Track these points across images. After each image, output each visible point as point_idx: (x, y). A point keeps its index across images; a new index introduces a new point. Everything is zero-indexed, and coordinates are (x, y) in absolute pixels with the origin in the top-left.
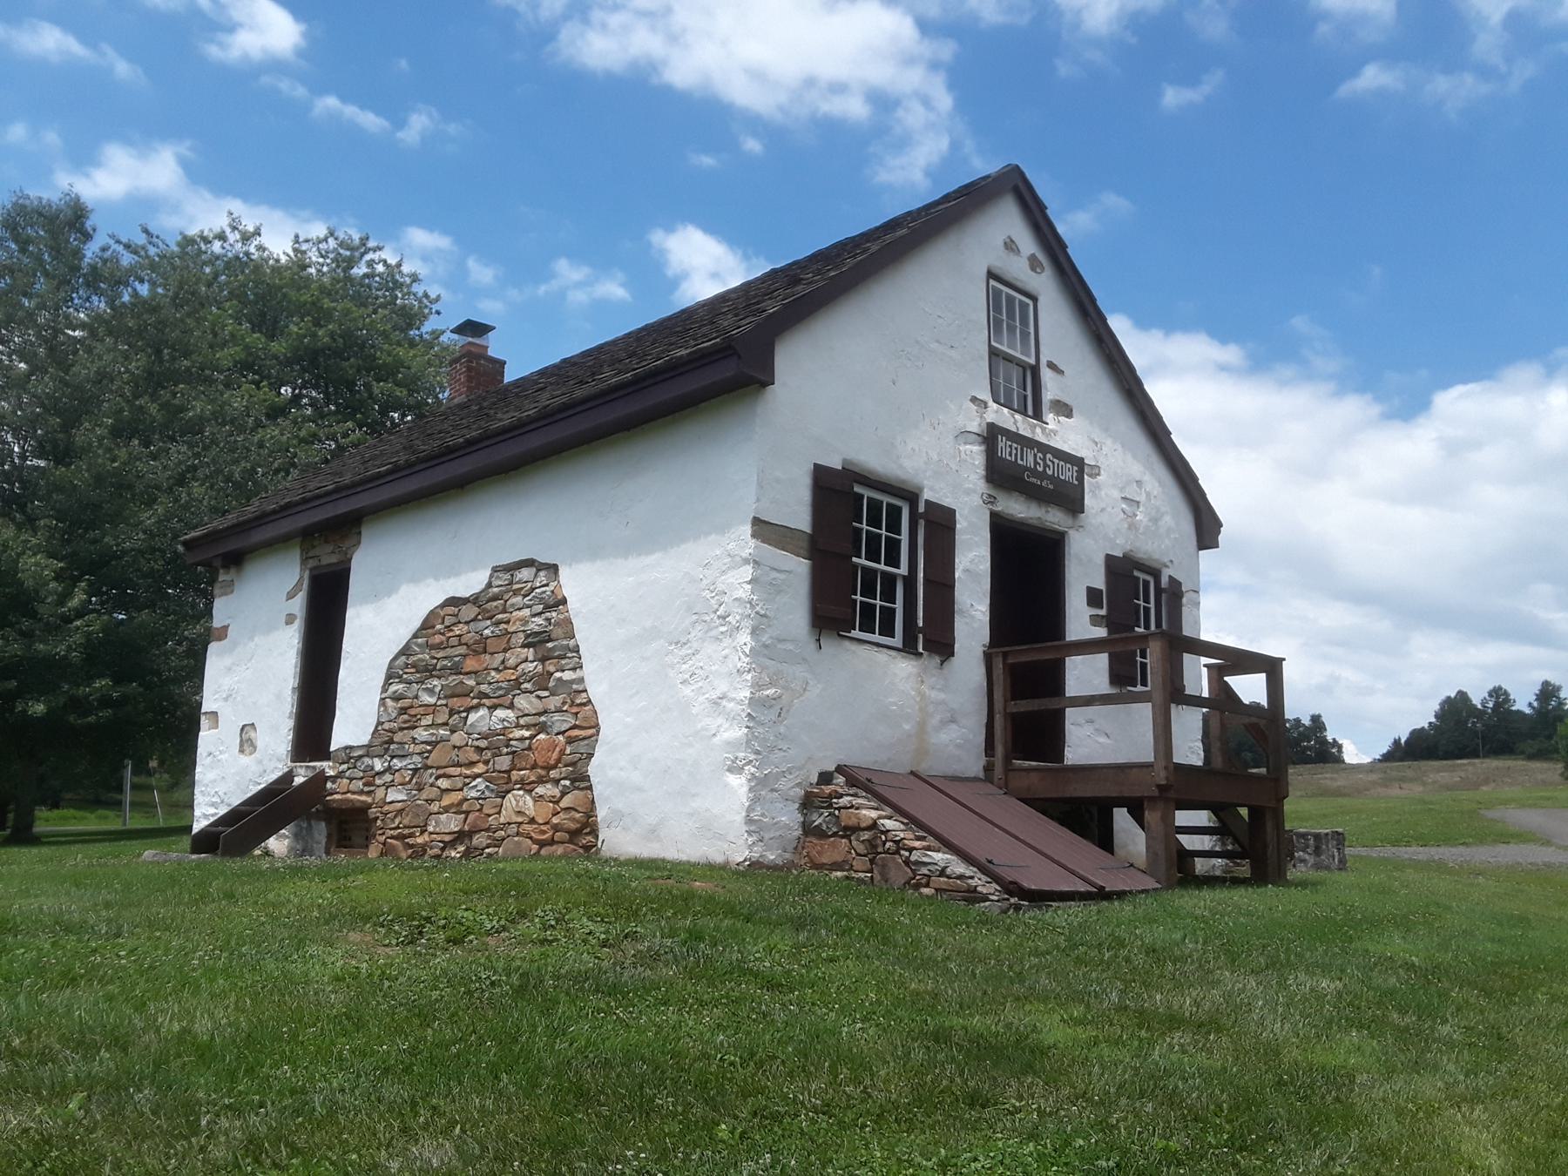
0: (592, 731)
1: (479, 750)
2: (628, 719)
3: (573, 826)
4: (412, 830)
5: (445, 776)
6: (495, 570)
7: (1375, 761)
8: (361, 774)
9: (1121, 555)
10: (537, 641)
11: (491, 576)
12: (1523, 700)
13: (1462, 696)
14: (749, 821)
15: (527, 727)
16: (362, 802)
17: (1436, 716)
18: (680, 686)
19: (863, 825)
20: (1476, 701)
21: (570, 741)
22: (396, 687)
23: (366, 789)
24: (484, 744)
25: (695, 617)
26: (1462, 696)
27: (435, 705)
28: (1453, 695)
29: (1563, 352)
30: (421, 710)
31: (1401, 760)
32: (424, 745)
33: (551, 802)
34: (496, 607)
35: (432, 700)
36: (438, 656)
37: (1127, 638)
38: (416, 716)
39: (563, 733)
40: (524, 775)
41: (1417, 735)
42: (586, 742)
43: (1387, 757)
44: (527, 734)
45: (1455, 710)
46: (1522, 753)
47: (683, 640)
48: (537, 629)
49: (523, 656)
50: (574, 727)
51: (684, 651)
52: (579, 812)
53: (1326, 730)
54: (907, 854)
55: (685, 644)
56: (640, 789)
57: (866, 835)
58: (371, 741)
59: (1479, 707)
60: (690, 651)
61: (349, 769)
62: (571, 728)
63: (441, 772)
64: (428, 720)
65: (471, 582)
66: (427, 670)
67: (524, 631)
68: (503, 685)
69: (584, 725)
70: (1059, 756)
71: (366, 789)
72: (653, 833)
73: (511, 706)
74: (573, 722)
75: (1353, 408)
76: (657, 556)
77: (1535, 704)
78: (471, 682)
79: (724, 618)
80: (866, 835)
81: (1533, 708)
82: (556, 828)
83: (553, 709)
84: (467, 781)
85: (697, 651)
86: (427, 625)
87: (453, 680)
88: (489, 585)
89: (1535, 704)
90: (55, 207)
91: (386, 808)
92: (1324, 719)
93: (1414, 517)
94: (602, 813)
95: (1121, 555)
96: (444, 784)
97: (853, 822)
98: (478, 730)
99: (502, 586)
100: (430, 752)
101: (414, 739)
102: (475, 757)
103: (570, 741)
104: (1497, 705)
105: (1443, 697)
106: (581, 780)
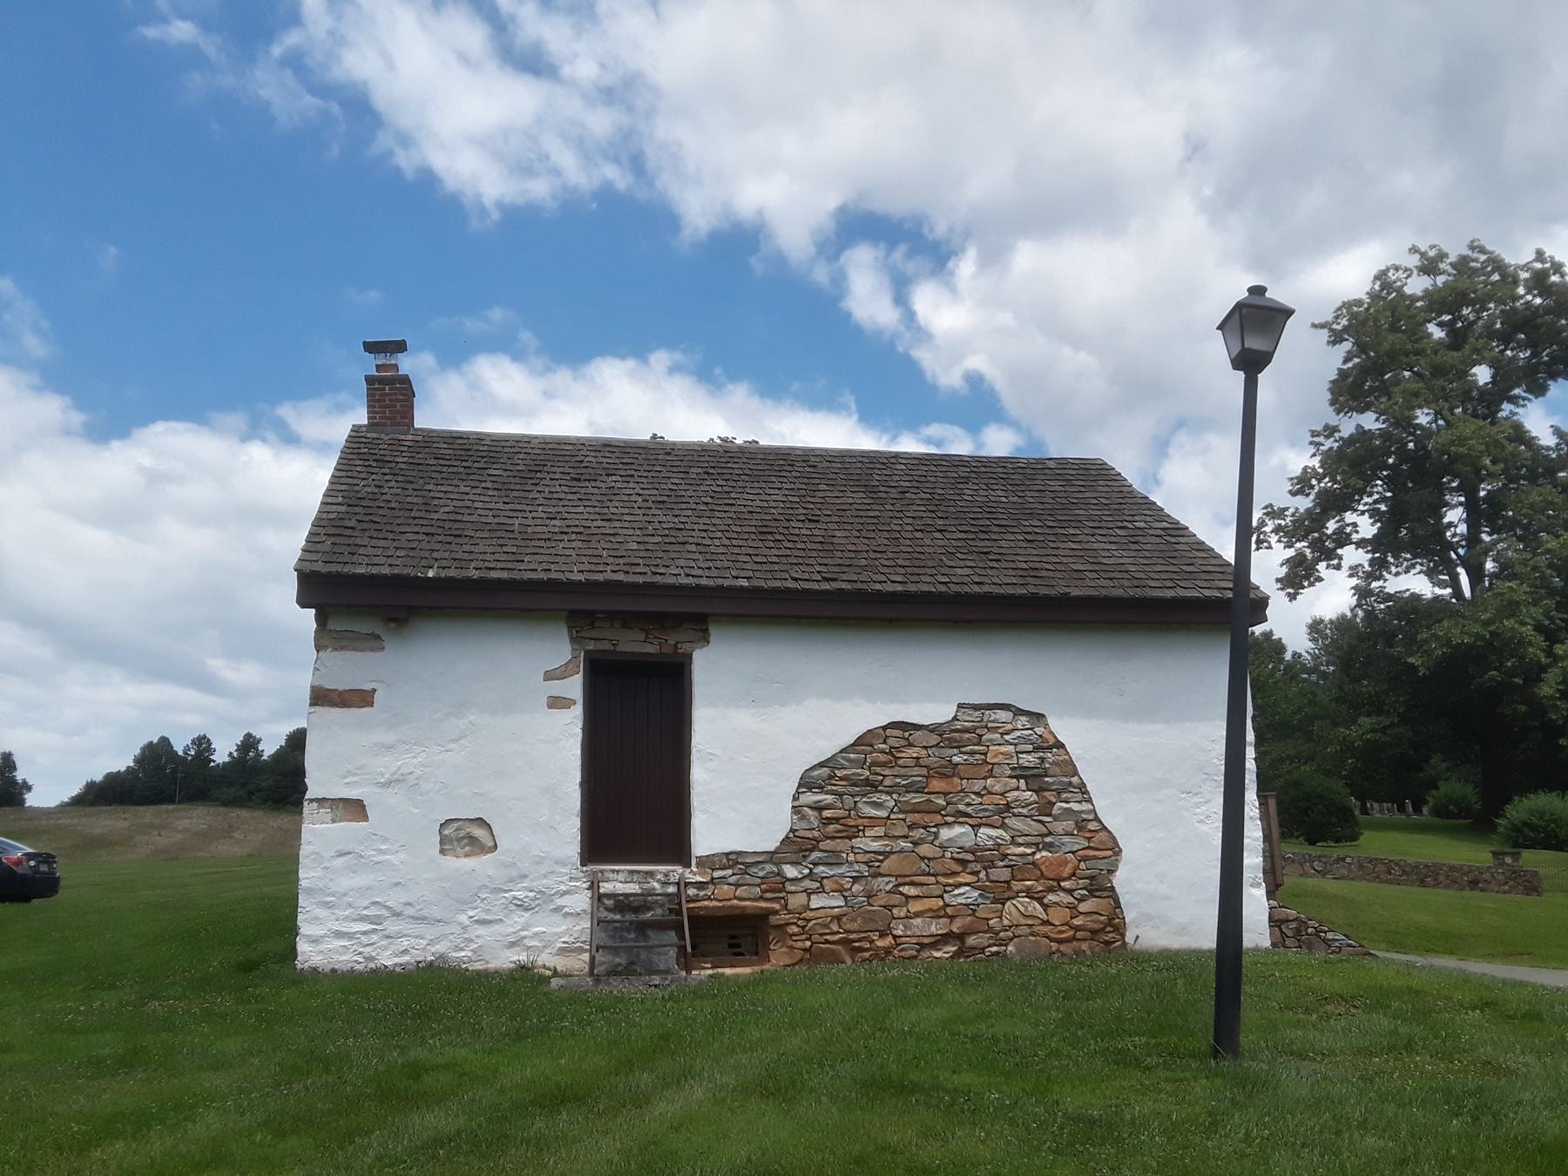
2: (1148, 845)
3: (1096, 926)
6: (960, 706)
7: (63, 806)
8: (759, 881)
11: (957, 711)
12: (223, 751)
13: (165, 741)
14: (1271, 919)
15: (1027, 845)
16: (761, 908)
17: (135, 761)
18: (1197, 824)
19: (1291, 918)
21: (1085, 859)
22: (809, 798)
25: (1205, 776)
26: (165, 741)
28: (155, 741)
31: (92, 804)
32: (872, 855)
33: (1067, 907)
34: (968, 739)
36: (885, 773)
39: (1073, 853)
40: (1033, 885)
41: (112, 778)
42: (1106, 861)
43: (78, 801)
44: (1029, 851)
45: (156, 755)
46: (217, 799)
47: (1196, 791)
48: (1027, 764)
51: (1196, 799)
52: (1102, 915)
53: (15, 769)
54: (1324, 935)
55: (1197, 794)
56: (1169, 898)
57: (1293, 925)
58: (778, 848)
59: (181, 753)
60: (1201, 800)
61: (734, 874)
62: (1083, 849)
65: (936, 711)
66: (873, 786)
67: (1008, 764)
68: (990, 807)
69: (1101, 847)
70: (675, 845)
72: (1183, 930)
73: (1003, 826)
74: (1087, 845)
75: (51, 408)
76: (1160, 726)
77: (235, 754)
78: (941, 802)
80: (1293, 925)
81: (233, 757)
82: (1077, 929)
83: (1062, 832)
85: (1210, 801)
88: (955, 718)
89: (235, 754)
90: (496, 216)
91: (809, 914)
92: (15, 758)
93: (97, 538)
94: (1129, 915)
96: (912, 891)
97: (1283, 917)
99: (973, 721)
100: (881, 861)
101: (852, 847)
102: (959, 869)
103: (1085, 859)
104: (199, 753)
105: (145, 742)
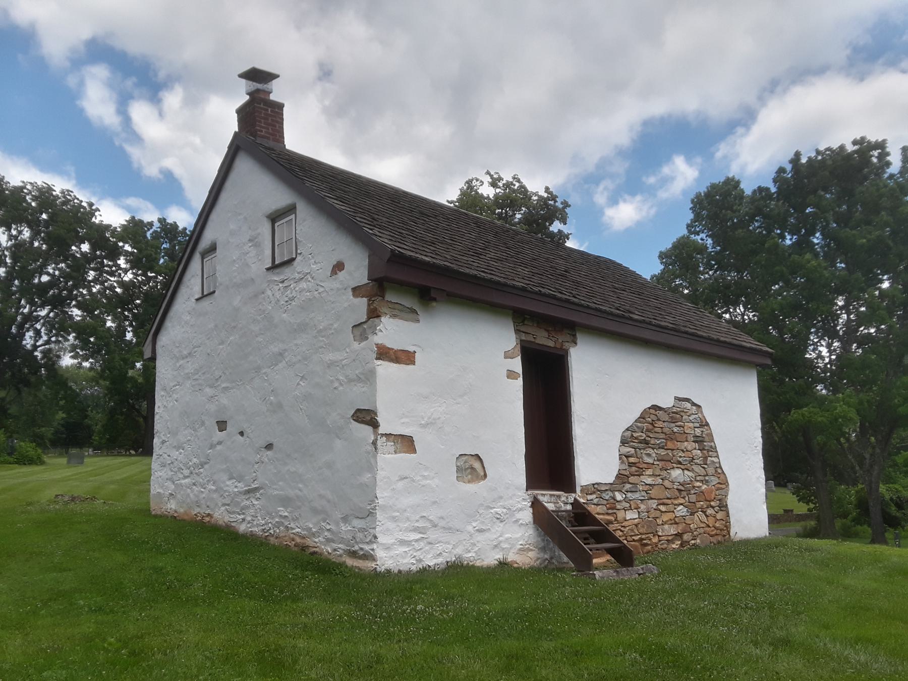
0: (723, 486)
1: (680, 491)
4: (647, 536)
5: (663, 504)
9: (248, 97)
10: (699, 440)
20: (748, 188)
23: (610, 511)
24: (681, 487)
27: (653, 464)
29: (907, 64)
30: (645, 466)
35: (651, 461)
37: (95, 476)
38: (642, 468)
49: (694, 446)
50: (719, 483)
63: (661, 501)
64: (649, 472)
71: (610, 511)
79: (756, 447)
84: (676, 507)
86: (642, 417)
87: (662, 452)
95: (248, 97)
98: (678, 481)
103: (718, 489)
106: (723, 507)
